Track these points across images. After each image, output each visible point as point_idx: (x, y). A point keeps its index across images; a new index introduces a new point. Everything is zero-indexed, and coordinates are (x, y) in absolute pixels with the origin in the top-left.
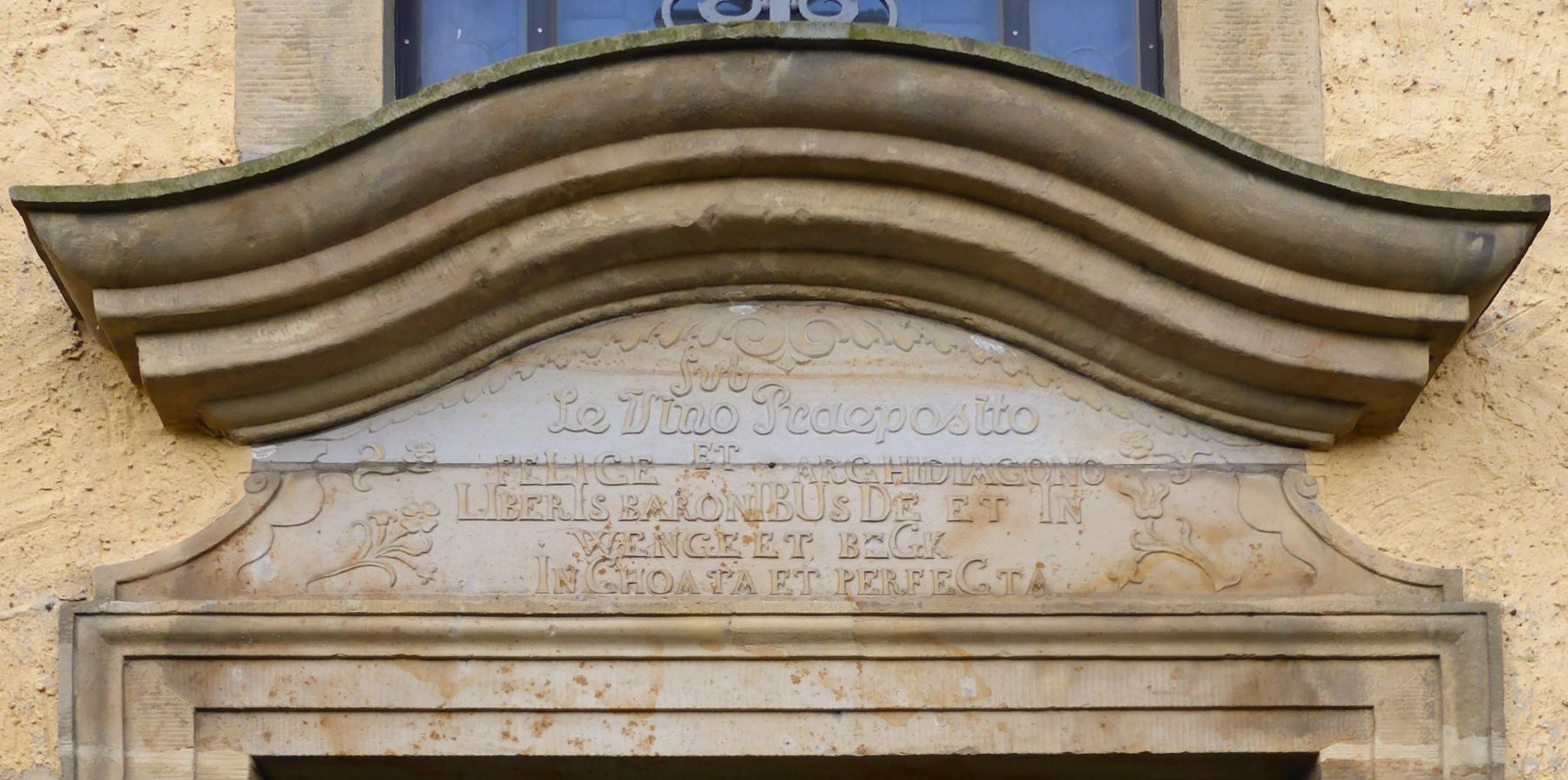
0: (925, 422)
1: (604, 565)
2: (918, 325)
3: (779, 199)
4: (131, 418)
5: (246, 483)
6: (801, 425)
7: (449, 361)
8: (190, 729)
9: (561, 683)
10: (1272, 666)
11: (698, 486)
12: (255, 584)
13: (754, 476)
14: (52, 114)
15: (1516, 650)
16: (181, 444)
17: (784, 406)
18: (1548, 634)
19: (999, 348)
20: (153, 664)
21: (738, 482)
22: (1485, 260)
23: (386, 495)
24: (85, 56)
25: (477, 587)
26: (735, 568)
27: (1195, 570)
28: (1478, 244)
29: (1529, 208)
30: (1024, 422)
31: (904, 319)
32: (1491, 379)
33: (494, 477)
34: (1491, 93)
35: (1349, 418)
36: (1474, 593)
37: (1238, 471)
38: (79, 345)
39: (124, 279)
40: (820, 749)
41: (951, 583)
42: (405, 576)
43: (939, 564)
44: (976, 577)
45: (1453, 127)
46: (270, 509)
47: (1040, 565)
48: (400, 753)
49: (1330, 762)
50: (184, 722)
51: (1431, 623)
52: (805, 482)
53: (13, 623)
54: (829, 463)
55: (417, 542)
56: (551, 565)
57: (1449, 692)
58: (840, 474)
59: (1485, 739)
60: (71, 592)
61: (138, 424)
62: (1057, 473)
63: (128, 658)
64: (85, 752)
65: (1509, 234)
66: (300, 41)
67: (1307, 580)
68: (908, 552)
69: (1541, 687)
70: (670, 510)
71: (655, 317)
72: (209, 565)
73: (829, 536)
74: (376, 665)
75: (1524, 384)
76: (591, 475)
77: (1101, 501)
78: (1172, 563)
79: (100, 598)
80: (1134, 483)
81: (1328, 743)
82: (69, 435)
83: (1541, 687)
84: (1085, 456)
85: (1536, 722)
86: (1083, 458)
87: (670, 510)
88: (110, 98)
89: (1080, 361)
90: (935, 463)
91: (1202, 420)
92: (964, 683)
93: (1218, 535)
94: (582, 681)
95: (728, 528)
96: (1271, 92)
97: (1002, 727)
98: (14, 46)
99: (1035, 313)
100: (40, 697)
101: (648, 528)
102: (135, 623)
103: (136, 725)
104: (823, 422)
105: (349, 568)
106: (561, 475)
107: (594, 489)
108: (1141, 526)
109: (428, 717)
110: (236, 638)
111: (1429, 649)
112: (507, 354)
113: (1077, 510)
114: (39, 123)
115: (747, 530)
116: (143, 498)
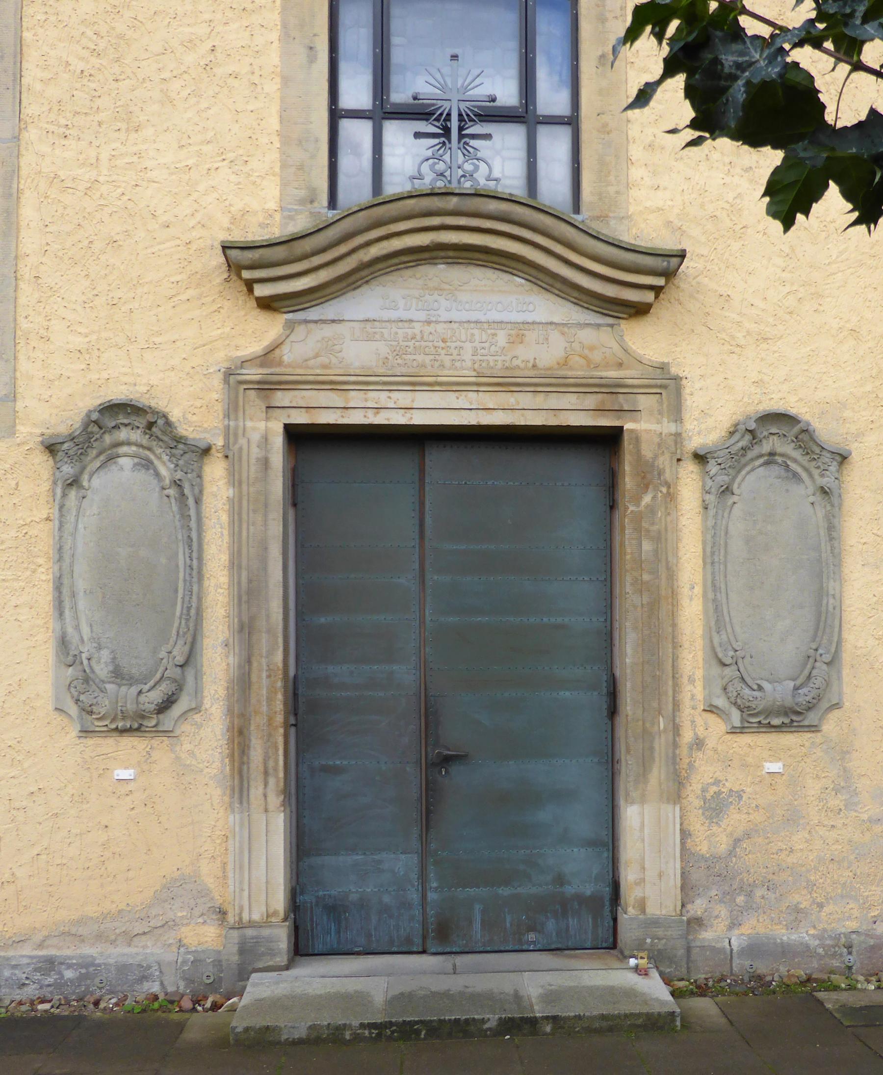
0: (500, 307)
1: (397, 357)
2: (497, 272)
3: (453, 237)
4: (246, 302)
5: (283, 326)
6: (460, 308)
7: (348, 285)
8: (264, 414)
9: (383, 398)
10: (609, 395)
11: (428, 329)
12: (286, 363)
13: (445, 326)
14: (220, 192)
15: (687, 391)
16: (262, 312)
17: (455, 301)
18: (698, 385)
19: (523, 281)
20: (253, 391)
21: (440, 328)
22: (668, 268)
23: (328, 331)
24: (230, 171)
25: (357, 364)
26: (439, 359)
27: (584, 360)
28: (665, 263)
29: (680, 253)
30: (531, 307)
31: (493, 271)
32: (681, 294)
33: (362, 325)
34: (683, 191)
35: (633, 311)
36: (674, 370)
37: (598, 326)
38: (229, 276)
39: (252, 267)
40: (465, 422)
41: (507, 365)
42: (334, 361)
43: (503, 358)
44: (516, 362)
45: (670, 203)
46: (291, 336)
47: (535, 359)
48: (331, 423)
49: (627, 430)
50: (262, 412)
51: (659, 382)
52: (461, 328)
53: (207, 376)
54: (469, 321)
55: (337, 348)
56: (381, 357)
57: (665, 406)
58: (472, 325)
59: (675, 424)
60: (226, 365)
61: (248, 305)
62: (541, 326)
63: (245, 389)
64: (232, 423)
65: (675, 261)
66: (301, 168)
67: (620, 365)
68: (493, 353)
69: (694, 405)
70: (418, 338)
71: (414, 269)
72: (271, 356)
73: (468, 346)
74: (27, 61)
75: (691, 296)
76: (393, 325)
77: (555, 336)
78: (577, 358)
79: (236, 368)
80: (566, 329)
81: (627, 423)
82: (226, 308)
83: (694, 405)
84: (550, 320)
85: (693, 417)
86: (549, 321)
87: (418, 338)
88: (240, 186)
89: (548, 287)
90: (501, 322)
91: (587, 308)
92: (511, 400)
93: (592, 348)
94: (390, 398)
95: (436, 344)
96: (612, 190)
97: (523, 415)
98: (207, 166)
99: (533, 272)
100: (216, 402)
101: (411, 344)
102: (248, 378)
103: (247, 413)
104: (467, 306)
105: (316, 356)
106: (384, 324)
107: (394, 329)
108: (568, 345)
109: (341, 410)
110: (280, 383)
111: (659, 391)
112: (367, 282)
113: (547, 339)
114: (215, 195)
115: (441, 344)
116: (250, 331)
